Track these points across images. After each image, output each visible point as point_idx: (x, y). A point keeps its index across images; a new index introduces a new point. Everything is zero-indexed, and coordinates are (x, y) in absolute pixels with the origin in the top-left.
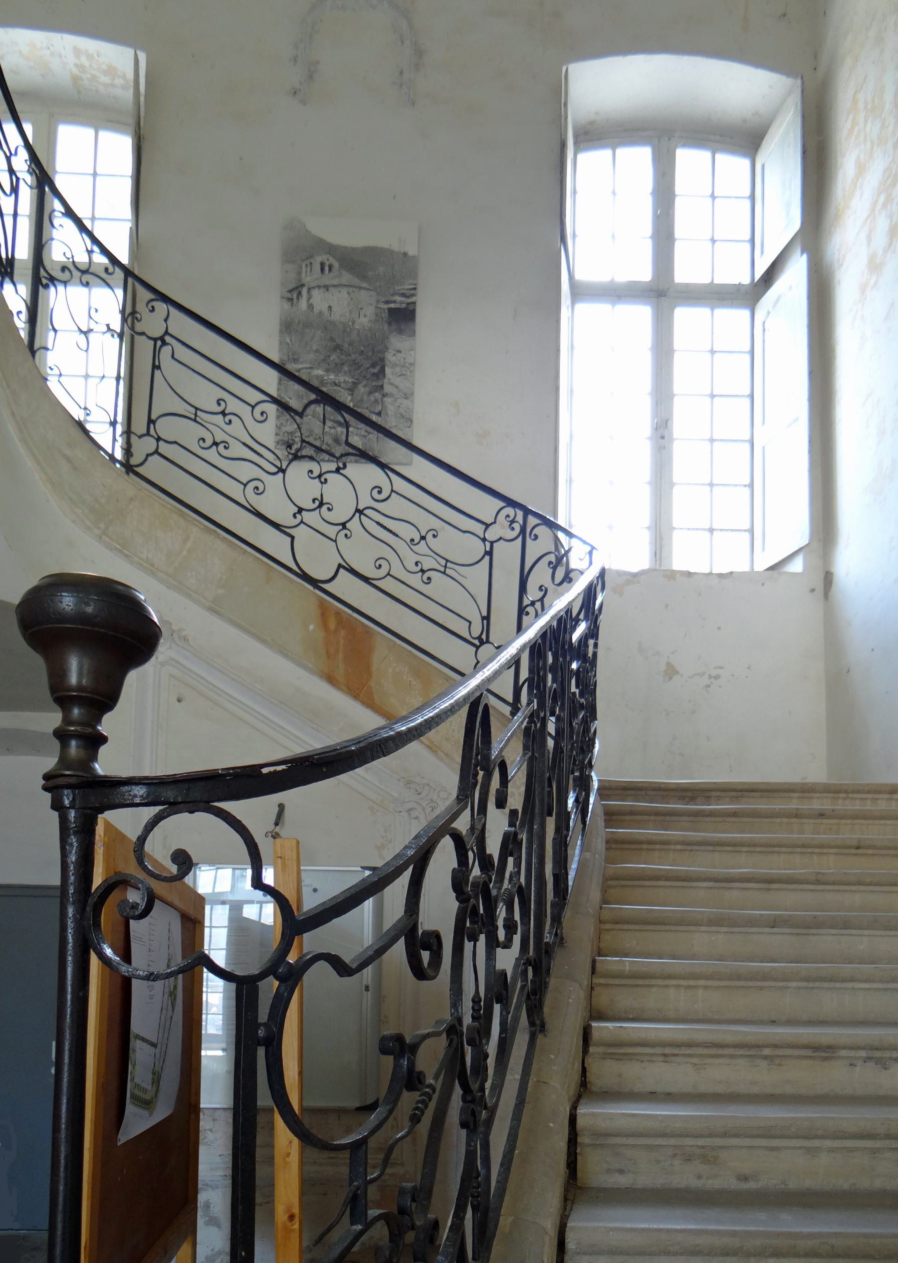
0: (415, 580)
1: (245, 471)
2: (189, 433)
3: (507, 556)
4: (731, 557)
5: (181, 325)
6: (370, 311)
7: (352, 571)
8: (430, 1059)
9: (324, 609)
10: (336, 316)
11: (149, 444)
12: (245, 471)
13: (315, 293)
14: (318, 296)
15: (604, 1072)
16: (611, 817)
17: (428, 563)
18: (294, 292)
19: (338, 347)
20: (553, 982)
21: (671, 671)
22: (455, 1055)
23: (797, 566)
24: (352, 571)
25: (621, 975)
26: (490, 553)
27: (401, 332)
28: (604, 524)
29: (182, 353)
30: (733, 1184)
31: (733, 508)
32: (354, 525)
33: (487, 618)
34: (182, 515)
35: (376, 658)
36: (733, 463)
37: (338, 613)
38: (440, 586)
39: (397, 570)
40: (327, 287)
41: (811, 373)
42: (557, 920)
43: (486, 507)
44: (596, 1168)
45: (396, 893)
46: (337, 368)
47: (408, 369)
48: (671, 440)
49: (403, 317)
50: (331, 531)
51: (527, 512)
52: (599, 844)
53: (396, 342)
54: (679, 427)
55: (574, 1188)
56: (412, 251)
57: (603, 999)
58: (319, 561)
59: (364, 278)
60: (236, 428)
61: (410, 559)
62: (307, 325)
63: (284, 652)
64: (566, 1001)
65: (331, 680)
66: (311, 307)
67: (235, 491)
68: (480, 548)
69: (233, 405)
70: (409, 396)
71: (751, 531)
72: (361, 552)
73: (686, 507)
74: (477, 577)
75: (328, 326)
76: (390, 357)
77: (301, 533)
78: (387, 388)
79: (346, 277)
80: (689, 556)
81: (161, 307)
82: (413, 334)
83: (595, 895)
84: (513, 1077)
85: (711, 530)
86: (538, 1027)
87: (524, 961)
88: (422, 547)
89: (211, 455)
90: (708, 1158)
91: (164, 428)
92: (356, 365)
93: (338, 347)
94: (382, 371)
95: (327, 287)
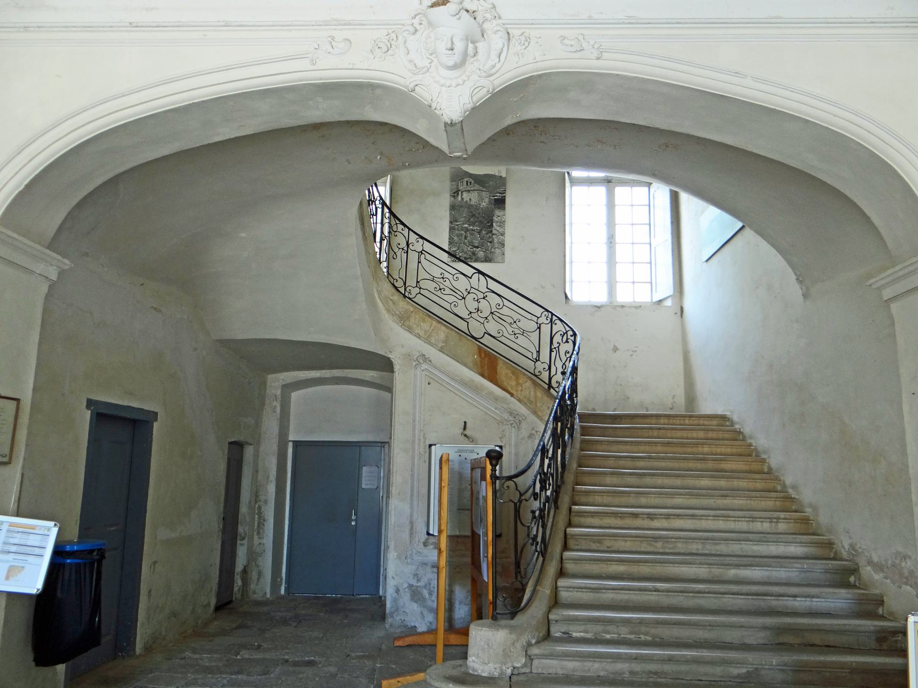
0: (512, 337)
1: (451, 299)
2: (431, 285)
3: (546, 329)
4: (643, 296)
5: (428, 247)
6: (487, 200)
7: (490, 335)
8: (537, 513)
9: (480, 349)
10: (472, 203)
11: (417, 290)
12: (451, 299)
13: (465, 194)
14: (465, 194)
15: (575, 520)
16: (585, 431)
17: (517, 331)
18: (455, 193)
19: (473, 215)
20: (561, 495)
21: (615, 349)
22: (540, 514)
23: (669, 303)
24: (490, 335)
25: (581, 492)
26: (539, 328)
27: (499, 208)
28: (585, 285)
29: (428, 256)
30: (606, 549)
31: (642, 273)
32: (490, 318)
33: (538, 352)
34: (429, 316)
35: (498, 368)
36: (642, 253)
37: (485, 351)
38: (521, 340)
39: (506, 334)
40: (469, 191)
41: (672, 222)
42: (562, 477)
43: (538, 311)
44: (571, 543)
45: (531, 490)
46: (473, 224)
47: (502, 223)
48: (615, 243)
49: (500, 203)
50: (482, 320)
51: (553, 314)
52: (577, 445)
53: (498, 212)
54: (618, 238)
55: (565, 547)
56: (504, 175)
57: (577, 499)
58: (477, 331)
59: (483, 187)
60: (447, 283)
61: (510, 330)
62: (462, 206)
63: (465, 365)
64: (565, 500)
65: (483, 376)
66: (462, 199)
67: (447, 306)
68: (536, 326)
69: (446, 275)
70: (503, 234)
71: (651, 283)
72: (492, 327)
73: (621, 272)
74: (535, 337)
75: (469, 206)
76: (495, 219)
77: (471, 321)
78: (494, 232)
79: (477, 187)
80: (624, 296)
81: (420, 240)
82: (504, 209)
83: (575, 465)
84: (551, 520)
85: (634, 283)
86: (557, 507)
87: (552, 493)
88: (514, 326)
89: (439, 293)
90: (599, 542)
91: (422, 284)
92: (481, 222)
93: (473, 215)
94: (492, 225)
95: (469, 191)
